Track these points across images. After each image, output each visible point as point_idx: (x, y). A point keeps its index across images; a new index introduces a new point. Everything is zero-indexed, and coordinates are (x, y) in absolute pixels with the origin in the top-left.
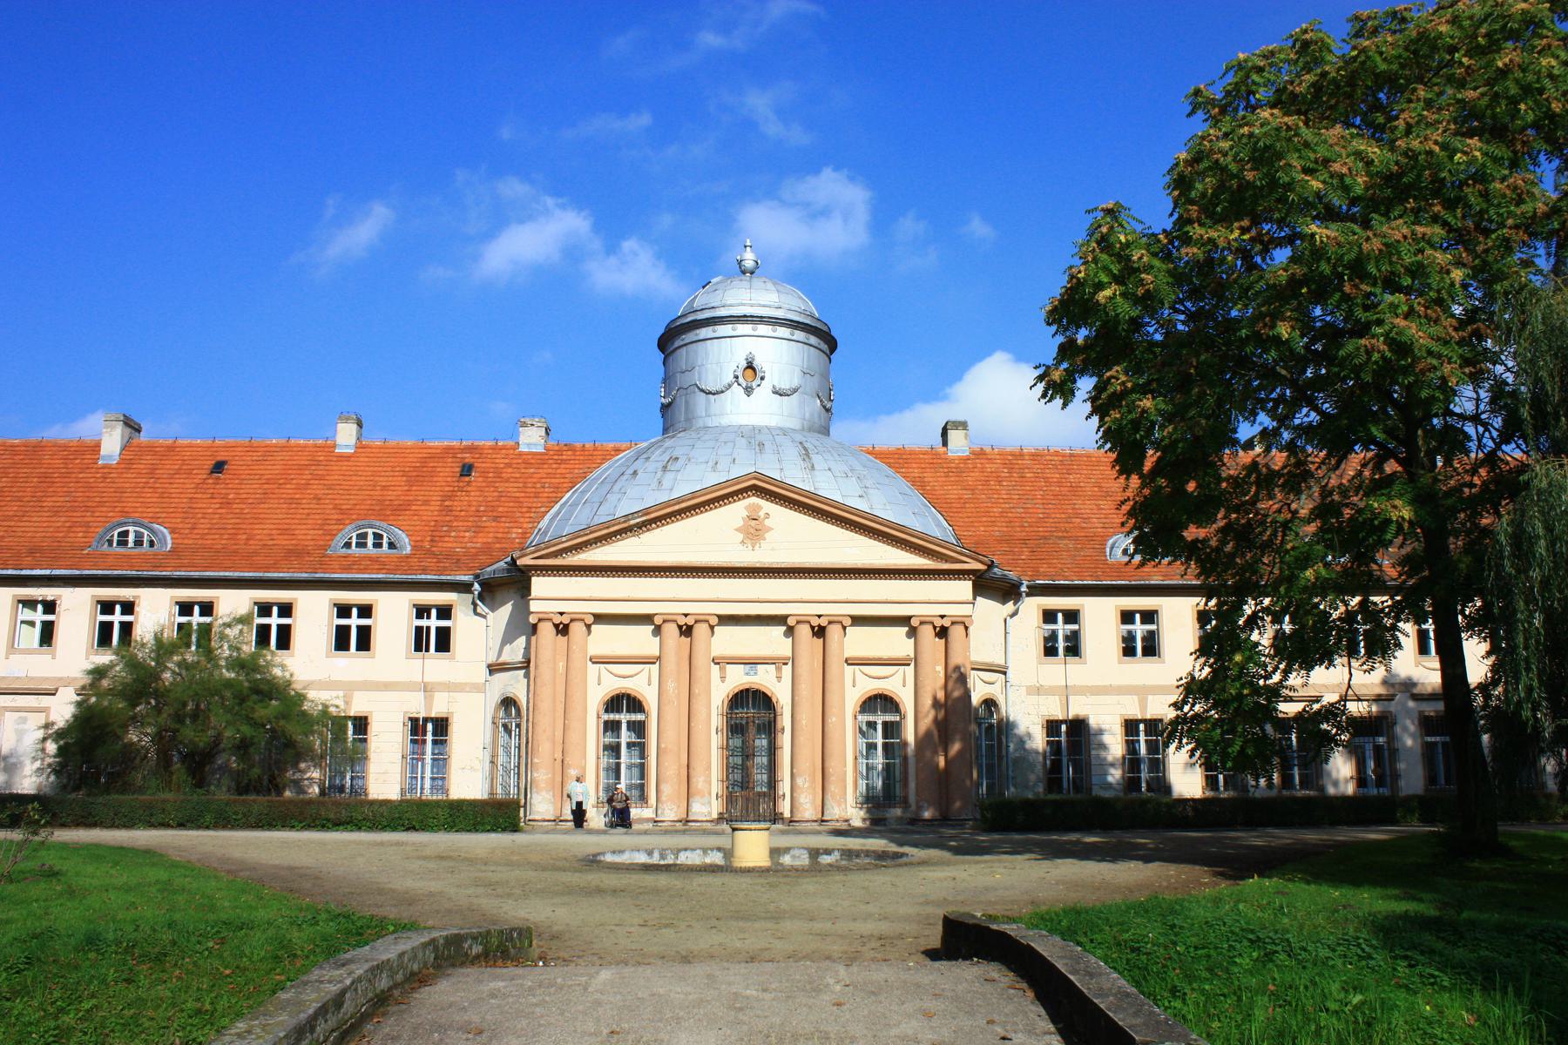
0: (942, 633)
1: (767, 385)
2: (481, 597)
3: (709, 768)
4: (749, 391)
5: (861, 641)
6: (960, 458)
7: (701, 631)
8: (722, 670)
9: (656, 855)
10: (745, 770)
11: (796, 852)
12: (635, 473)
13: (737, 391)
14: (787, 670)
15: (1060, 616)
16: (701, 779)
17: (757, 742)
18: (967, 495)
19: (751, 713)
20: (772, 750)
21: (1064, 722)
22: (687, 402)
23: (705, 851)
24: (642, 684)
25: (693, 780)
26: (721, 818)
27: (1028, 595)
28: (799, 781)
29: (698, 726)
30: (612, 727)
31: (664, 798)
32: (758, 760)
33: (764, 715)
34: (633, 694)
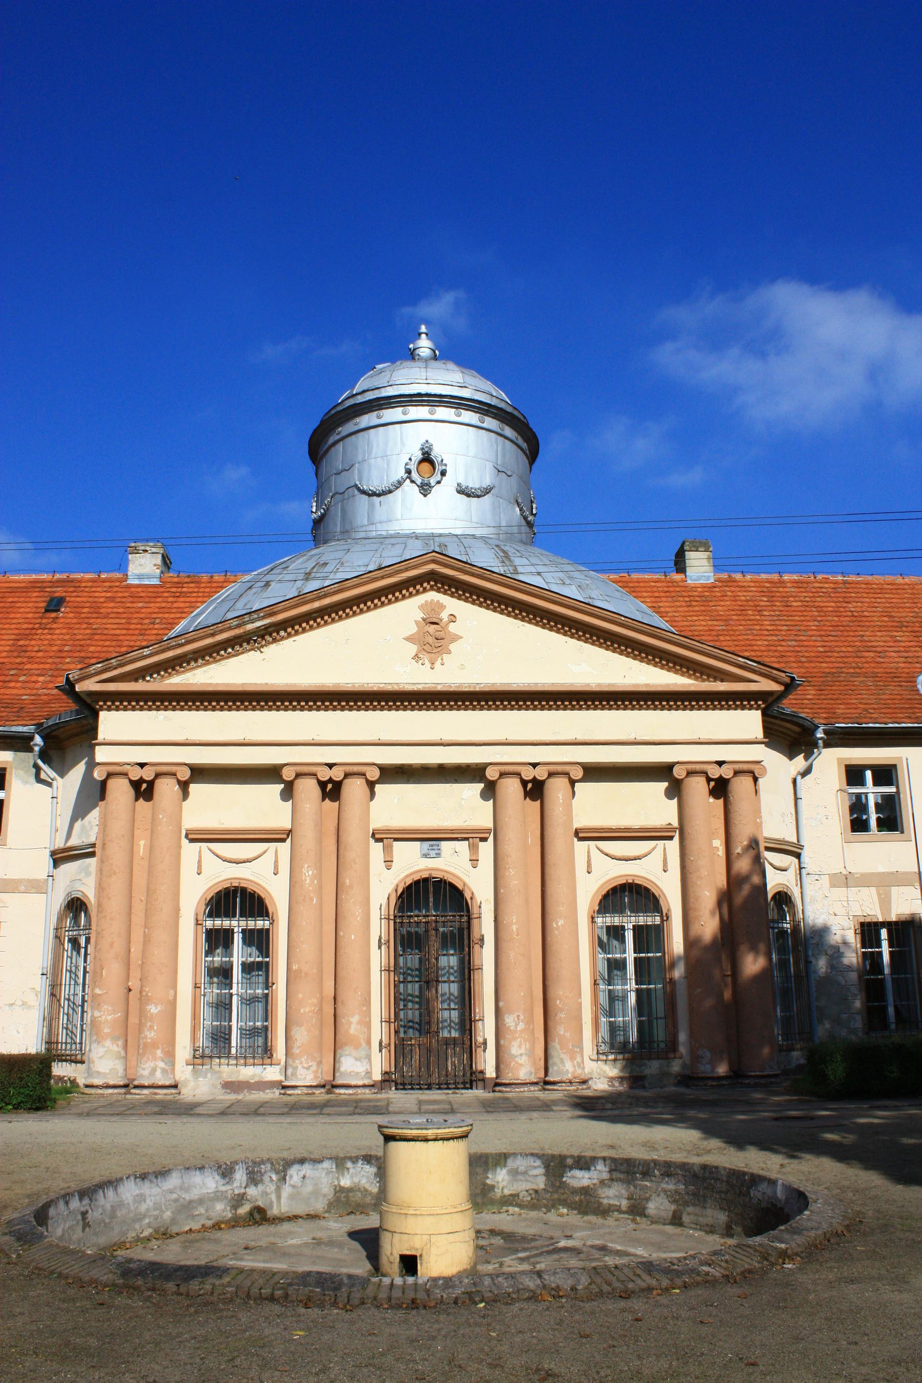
0: (720, 788)
1: (449, 483)
2: (44, 755)
3: (367, 1002)
4: (425, 489)
5: (596, 804)
6: (704, 586)
7: (354, 789)
8: (388, 850)
9: (240, 1175)
10: (425, 1005)
11: (520, 1163)
12: (267, 584)
13: (410, 490)
14: (486, 849)
15: (869, 774)
16: (355, 1019)
17: (443, 961)
18: (719, 626)
19: (432, 914)
20: (466, 973)
21: (883, 924)
22: (344, 511)
23: (340, 1162)
24: (266, 872)
25: (342, 1021)
26: (387, 1081)
27: (827, 745)
28: (509, 1020)
29: (351, 936)
30: (218, 940)
31: (296, 1051)
32: (443, 988)
33: (449, 922)
34: (251, 887)
